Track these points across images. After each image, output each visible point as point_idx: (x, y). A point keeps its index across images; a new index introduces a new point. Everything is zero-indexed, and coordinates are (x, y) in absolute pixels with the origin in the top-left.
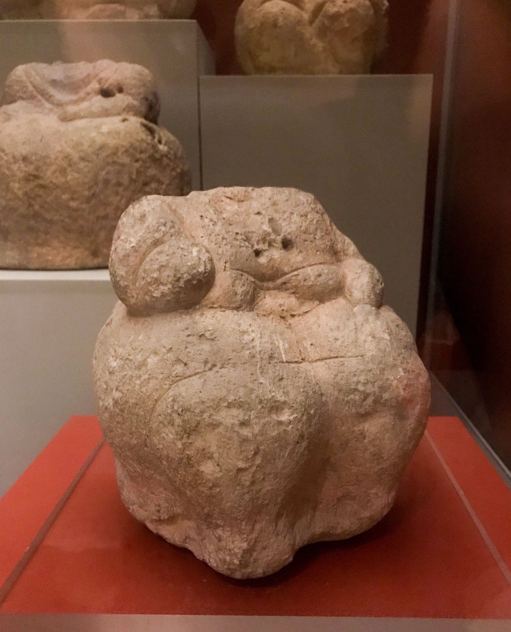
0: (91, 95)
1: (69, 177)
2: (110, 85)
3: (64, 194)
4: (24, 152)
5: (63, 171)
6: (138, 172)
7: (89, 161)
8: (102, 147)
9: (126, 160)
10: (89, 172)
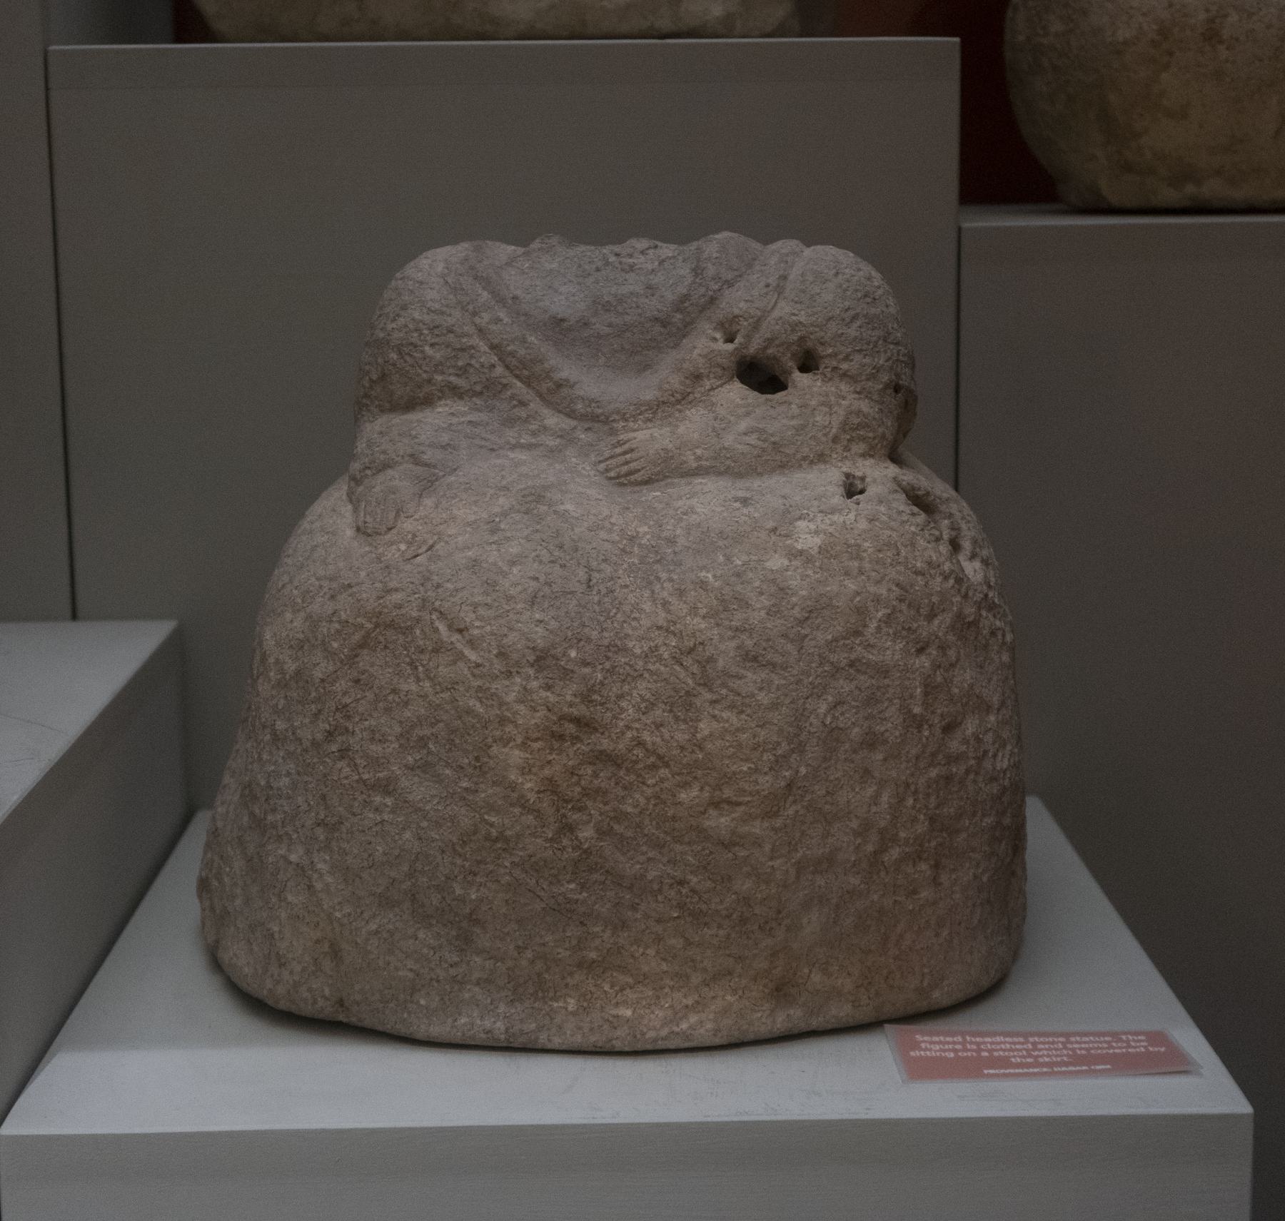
0: (707, 384)
1: (705, 727)
2: (770, 341)
3: (685, 785)
4: (540, 636)
5: (683, 705)
6: (930, 689)
7: (773, 666)
8: (816, 609)
9: (891, 651)
10: (775, 706)
